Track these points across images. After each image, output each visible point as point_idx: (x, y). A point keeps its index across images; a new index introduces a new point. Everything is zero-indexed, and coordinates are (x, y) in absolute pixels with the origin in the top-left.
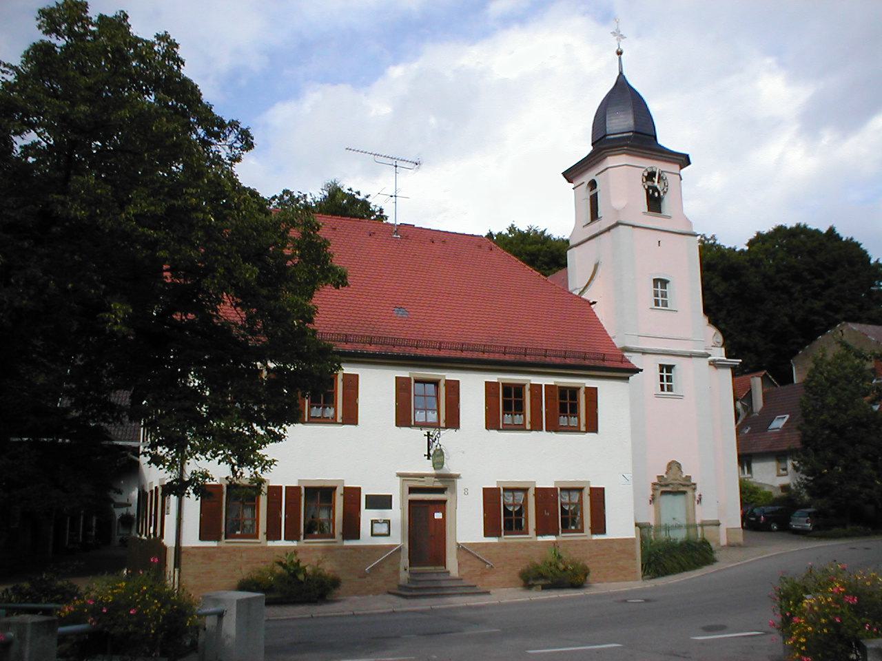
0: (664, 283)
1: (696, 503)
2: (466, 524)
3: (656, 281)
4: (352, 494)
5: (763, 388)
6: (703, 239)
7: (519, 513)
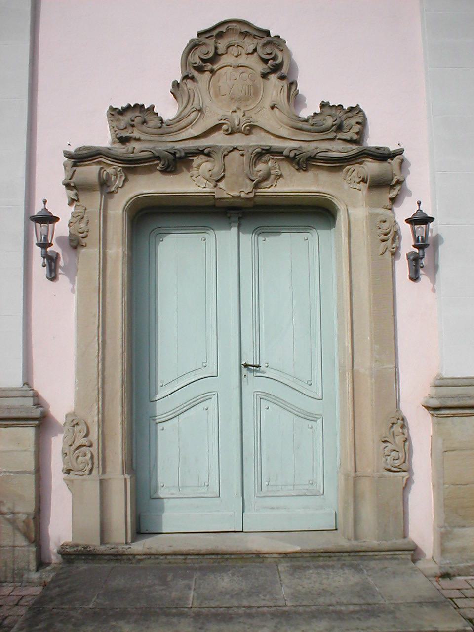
1: (402, 267)
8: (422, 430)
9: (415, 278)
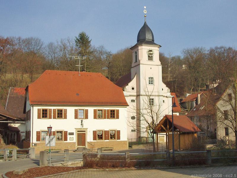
0: (152, 78)
2: (89, 138)
4: (66, 133)
7: (114, 135)
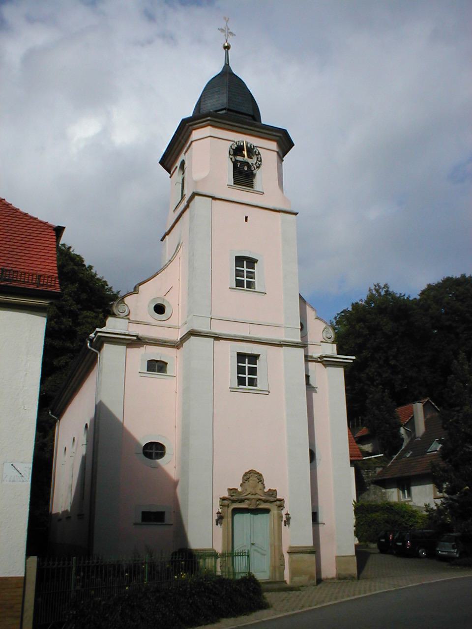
0: (251, 262)
1: (283, 523)
3: (239, 260)
5: (425, 416)
6: (377, 288)
8: (287, 557)
9: (285, 525)
